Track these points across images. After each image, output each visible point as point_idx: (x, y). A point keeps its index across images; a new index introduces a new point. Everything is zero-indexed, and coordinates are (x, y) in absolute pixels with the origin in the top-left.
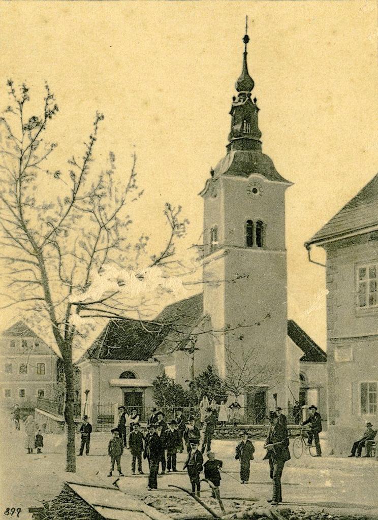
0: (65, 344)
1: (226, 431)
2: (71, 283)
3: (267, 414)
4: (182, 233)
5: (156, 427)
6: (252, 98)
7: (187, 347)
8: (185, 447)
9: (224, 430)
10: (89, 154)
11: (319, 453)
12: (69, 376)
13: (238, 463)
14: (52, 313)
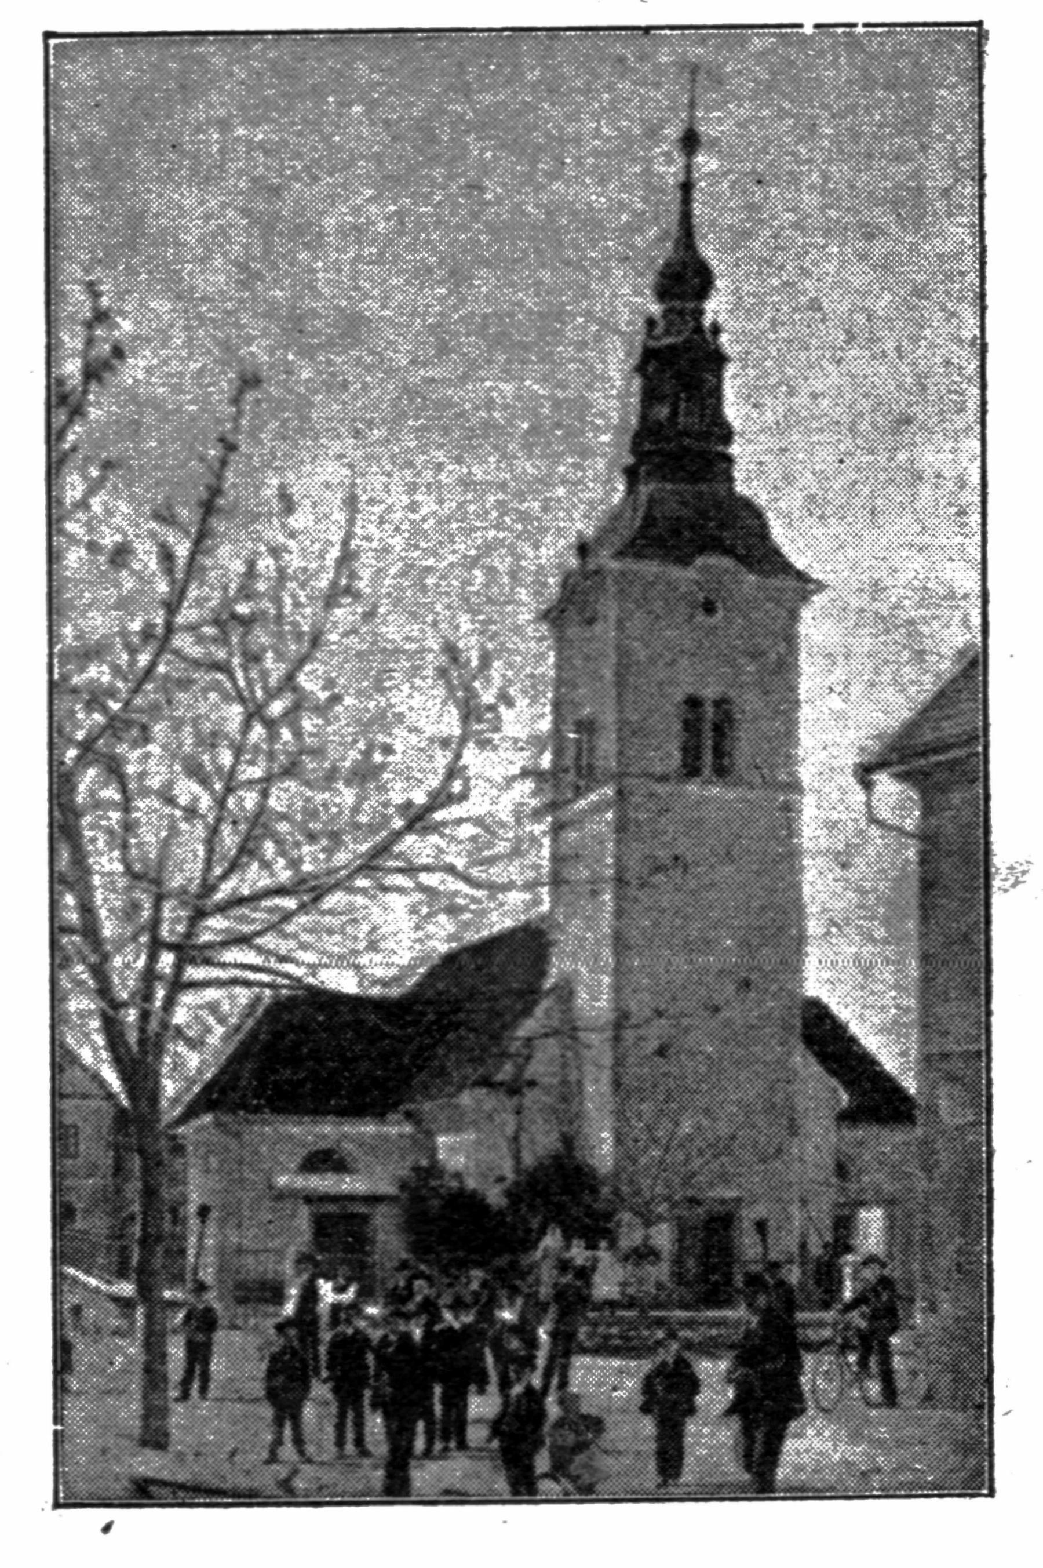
0: (138, 1066)
1: (614, 1330)
2: (158, 882)
3: (739, 1280)
4: (488, 735)
5: (407, 1317)
6: (707, 321)
7: (500, 1077)
8: (494, 1377)
9: (609, 1325)
10: (216, 491)
11: (890, 1396)
12: (152, 1164)
13: (648, 1426)
14: (100, 972)
